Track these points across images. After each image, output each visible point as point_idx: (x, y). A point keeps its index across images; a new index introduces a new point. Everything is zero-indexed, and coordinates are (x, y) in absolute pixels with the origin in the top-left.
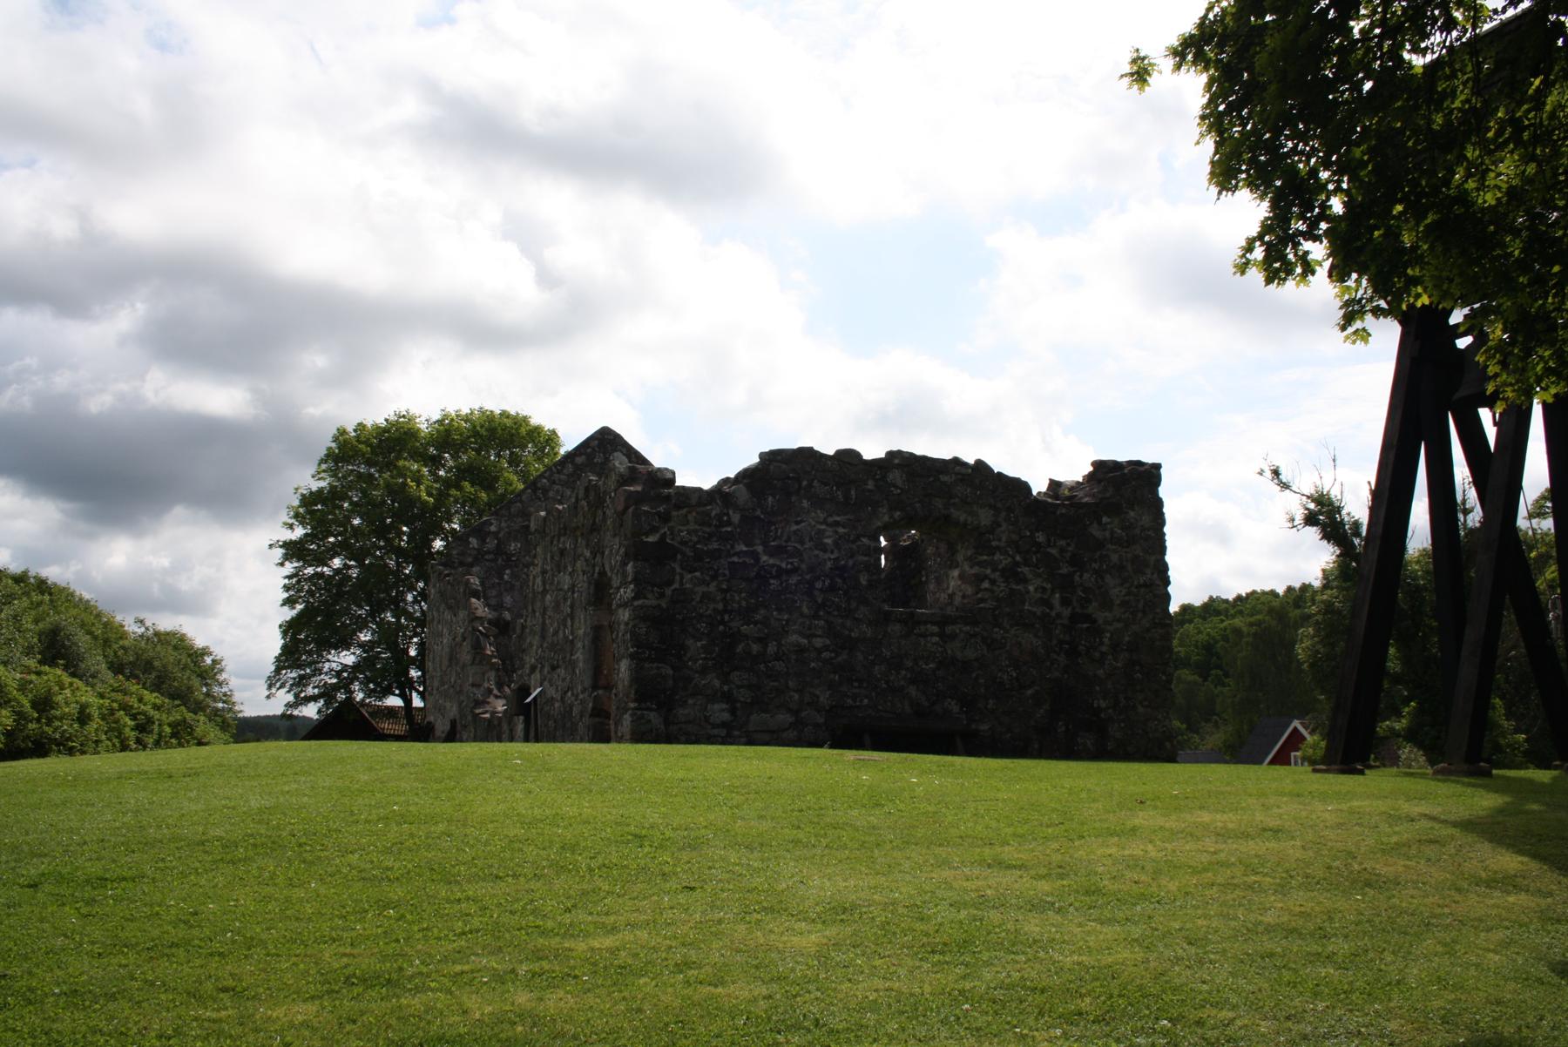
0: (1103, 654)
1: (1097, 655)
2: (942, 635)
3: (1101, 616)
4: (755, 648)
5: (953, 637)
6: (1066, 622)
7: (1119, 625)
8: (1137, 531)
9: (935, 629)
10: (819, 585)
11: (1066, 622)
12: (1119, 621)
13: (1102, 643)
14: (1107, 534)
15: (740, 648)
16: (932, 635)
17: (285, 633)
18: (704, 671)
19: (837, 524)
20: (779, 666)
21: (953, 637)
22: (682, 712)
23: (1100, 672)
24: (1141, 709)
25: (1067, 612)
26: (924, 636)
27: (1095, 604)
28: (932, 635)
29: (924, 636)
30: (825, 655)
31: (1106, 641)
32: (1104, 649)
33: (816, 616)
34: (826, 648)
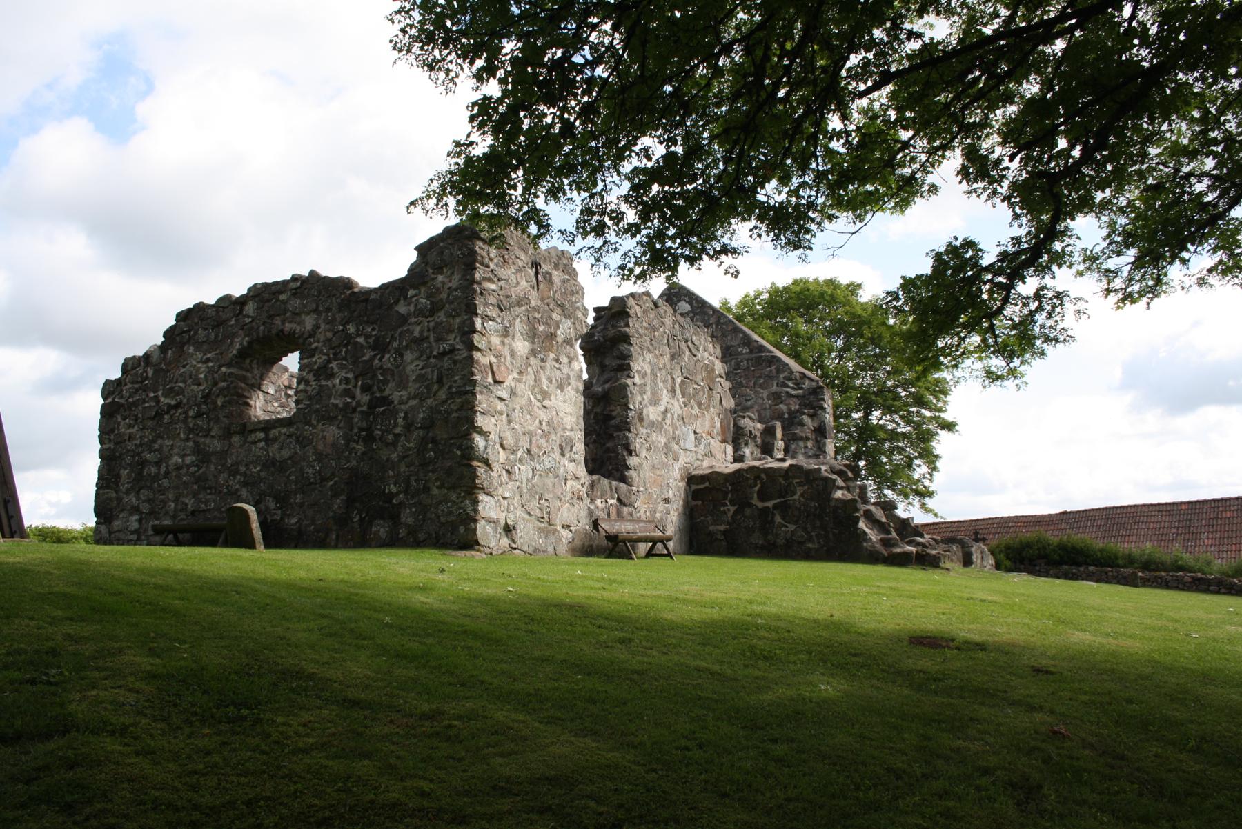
0: (397, 436)
1: (391, 437)
2: (266, 440)
3: (396, 396)
4: (153, 470)
5: (275, 440)
6: (365, 408)
7: (413, 403)
8: (444, 296)
9: (262, 435)
10: (191, 413)
11: (365, 408)
12: (414, 398)
13: (396, 425)
14: (412, 308)
15: (678, 241)
16: (260, 441)
17: (105, 395)
18: (128, 492)
19: (208, 360)
20: (165, 482)
21: (275, 440)
22: (117, 524)
23: (394, 456)
24: (435, 491)
25: (366, 398)
26: (254, 443)
27: (391, 385)
28: (260, 441)
29: (254, 443)
30: (193, 469)
31: (400, 421)
32: (398, 431)
33: (188, 439)
34: (192, 464)
